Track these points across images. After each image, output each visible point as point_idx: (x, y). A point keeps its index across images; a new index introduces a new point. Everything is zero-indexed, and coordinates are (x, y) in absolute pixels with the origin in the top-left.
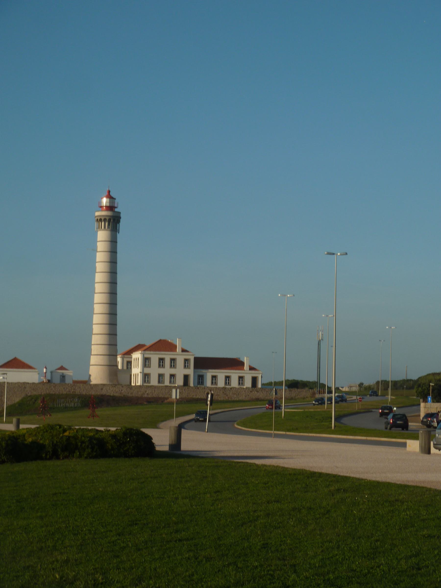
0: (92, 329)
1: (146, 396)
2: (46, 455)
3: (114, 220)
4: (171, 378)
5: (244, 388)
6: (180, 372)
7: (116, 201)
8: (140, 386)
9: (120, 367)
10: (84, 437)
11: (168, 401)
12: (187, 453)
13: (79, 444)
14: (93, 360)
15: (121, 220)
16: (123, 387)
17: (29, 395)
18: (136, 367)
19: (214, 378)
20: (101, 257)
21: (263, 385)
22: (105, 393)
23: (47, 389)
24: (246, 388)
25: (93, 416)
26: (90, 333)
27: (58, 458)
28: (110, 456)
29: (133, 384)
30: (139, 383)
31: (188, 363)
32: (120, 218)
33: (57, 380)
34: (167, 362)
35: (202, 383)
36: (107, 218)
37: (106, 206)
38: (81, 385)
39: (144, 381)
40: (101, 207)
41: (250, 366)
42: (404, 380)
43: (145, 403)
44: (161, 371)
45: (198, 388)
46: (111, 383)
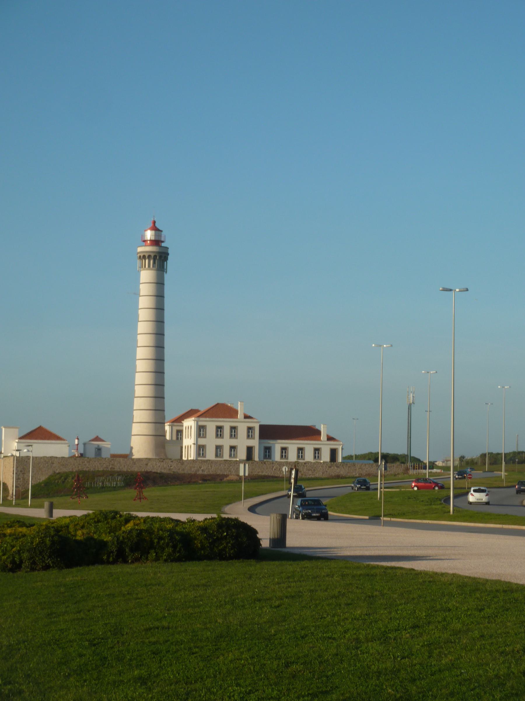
0: (134, 391)
1: (200, 472)
2: (108, 557)
3: (160, 257)
4: (231, 450)
5: (321, 463)
6: (242, 443)
7: (163, 233)
8: (193, 460)
9: (168, 437)
10: (162, 530)
11: (228, 478)
12: (297, 551)
13: (156, 541)
14: (136, 429)
15: (169, 257)
16: (172, 462)
17: (57, 472)
18: (188, 437)
19: (284, 450)
20: (145, 303)
21: (343, 458)
22: (150, 470)
23: (79, 464)
24: (324, 462)
25: (140, 499)
26: (132, 396)
27: (125, 561)
28: (200, 559)
29: (184, 458)
30: (192, 456)
31: (252, 432)
32: (168, 254)
33: (91, 454)
34: (227, 431)
35: (270, 457)
36: (152, 255)
37: (150, 240)
38: (121, 459)
39: (198, 454)
40: (145, 241)
41: (327, 436)
42: (514, 453)
43: (200, 482)
44: (219, 442)
45: (265, 463)
46: (157, 458)
